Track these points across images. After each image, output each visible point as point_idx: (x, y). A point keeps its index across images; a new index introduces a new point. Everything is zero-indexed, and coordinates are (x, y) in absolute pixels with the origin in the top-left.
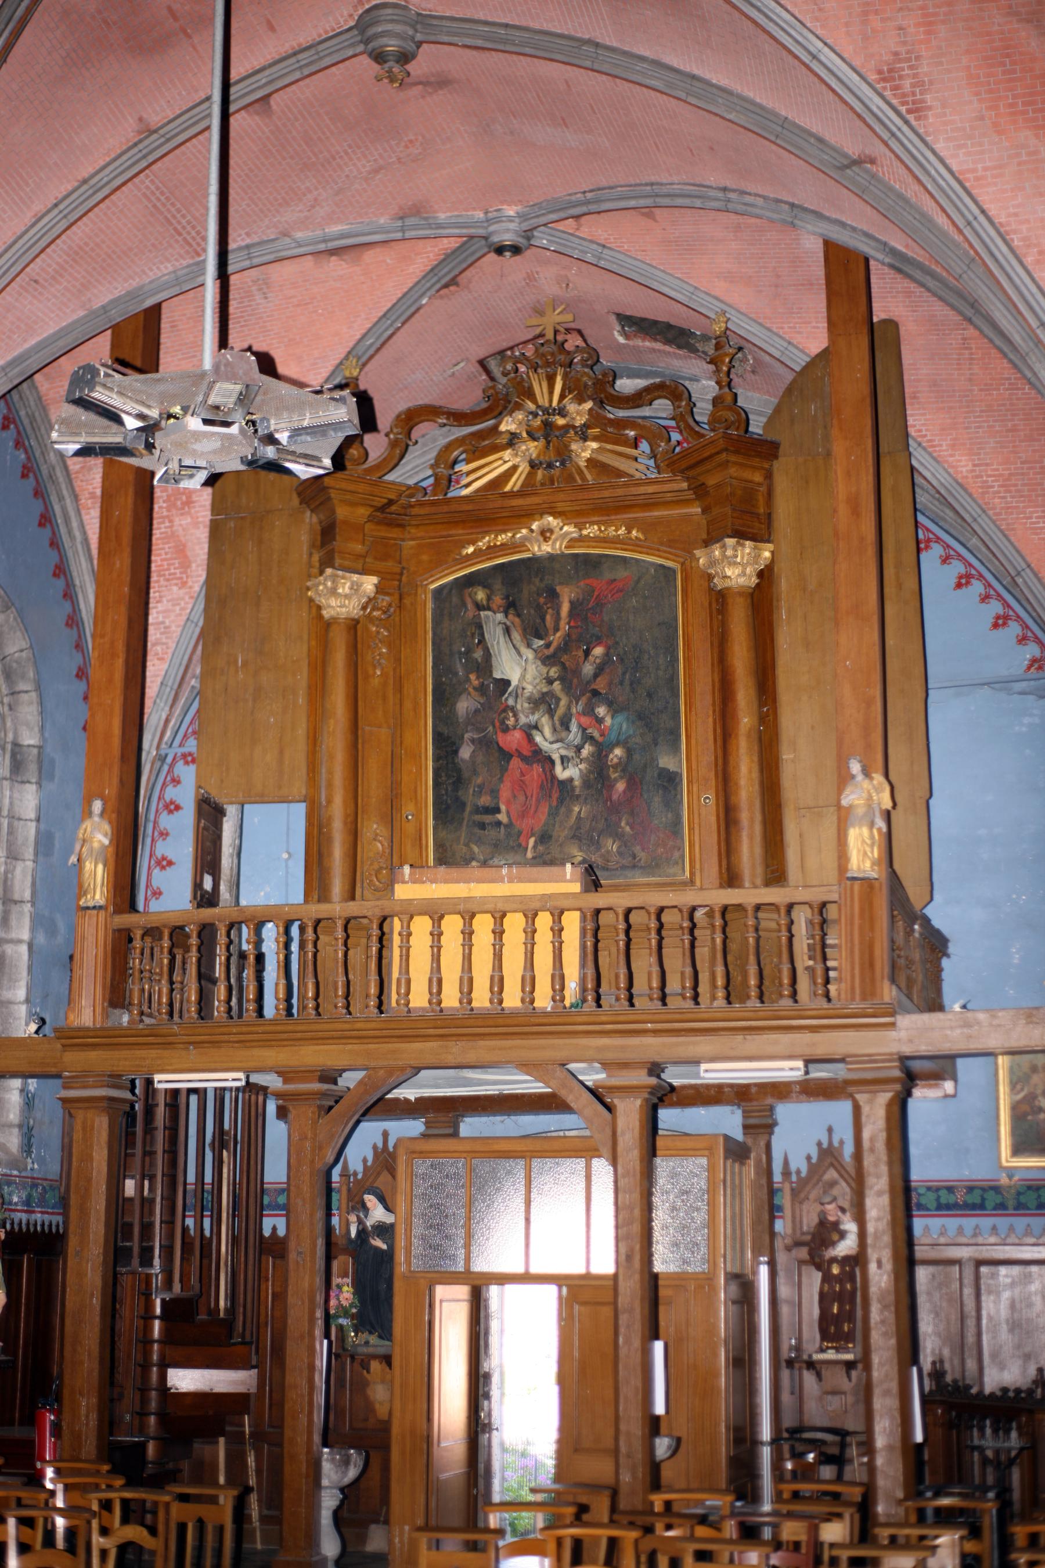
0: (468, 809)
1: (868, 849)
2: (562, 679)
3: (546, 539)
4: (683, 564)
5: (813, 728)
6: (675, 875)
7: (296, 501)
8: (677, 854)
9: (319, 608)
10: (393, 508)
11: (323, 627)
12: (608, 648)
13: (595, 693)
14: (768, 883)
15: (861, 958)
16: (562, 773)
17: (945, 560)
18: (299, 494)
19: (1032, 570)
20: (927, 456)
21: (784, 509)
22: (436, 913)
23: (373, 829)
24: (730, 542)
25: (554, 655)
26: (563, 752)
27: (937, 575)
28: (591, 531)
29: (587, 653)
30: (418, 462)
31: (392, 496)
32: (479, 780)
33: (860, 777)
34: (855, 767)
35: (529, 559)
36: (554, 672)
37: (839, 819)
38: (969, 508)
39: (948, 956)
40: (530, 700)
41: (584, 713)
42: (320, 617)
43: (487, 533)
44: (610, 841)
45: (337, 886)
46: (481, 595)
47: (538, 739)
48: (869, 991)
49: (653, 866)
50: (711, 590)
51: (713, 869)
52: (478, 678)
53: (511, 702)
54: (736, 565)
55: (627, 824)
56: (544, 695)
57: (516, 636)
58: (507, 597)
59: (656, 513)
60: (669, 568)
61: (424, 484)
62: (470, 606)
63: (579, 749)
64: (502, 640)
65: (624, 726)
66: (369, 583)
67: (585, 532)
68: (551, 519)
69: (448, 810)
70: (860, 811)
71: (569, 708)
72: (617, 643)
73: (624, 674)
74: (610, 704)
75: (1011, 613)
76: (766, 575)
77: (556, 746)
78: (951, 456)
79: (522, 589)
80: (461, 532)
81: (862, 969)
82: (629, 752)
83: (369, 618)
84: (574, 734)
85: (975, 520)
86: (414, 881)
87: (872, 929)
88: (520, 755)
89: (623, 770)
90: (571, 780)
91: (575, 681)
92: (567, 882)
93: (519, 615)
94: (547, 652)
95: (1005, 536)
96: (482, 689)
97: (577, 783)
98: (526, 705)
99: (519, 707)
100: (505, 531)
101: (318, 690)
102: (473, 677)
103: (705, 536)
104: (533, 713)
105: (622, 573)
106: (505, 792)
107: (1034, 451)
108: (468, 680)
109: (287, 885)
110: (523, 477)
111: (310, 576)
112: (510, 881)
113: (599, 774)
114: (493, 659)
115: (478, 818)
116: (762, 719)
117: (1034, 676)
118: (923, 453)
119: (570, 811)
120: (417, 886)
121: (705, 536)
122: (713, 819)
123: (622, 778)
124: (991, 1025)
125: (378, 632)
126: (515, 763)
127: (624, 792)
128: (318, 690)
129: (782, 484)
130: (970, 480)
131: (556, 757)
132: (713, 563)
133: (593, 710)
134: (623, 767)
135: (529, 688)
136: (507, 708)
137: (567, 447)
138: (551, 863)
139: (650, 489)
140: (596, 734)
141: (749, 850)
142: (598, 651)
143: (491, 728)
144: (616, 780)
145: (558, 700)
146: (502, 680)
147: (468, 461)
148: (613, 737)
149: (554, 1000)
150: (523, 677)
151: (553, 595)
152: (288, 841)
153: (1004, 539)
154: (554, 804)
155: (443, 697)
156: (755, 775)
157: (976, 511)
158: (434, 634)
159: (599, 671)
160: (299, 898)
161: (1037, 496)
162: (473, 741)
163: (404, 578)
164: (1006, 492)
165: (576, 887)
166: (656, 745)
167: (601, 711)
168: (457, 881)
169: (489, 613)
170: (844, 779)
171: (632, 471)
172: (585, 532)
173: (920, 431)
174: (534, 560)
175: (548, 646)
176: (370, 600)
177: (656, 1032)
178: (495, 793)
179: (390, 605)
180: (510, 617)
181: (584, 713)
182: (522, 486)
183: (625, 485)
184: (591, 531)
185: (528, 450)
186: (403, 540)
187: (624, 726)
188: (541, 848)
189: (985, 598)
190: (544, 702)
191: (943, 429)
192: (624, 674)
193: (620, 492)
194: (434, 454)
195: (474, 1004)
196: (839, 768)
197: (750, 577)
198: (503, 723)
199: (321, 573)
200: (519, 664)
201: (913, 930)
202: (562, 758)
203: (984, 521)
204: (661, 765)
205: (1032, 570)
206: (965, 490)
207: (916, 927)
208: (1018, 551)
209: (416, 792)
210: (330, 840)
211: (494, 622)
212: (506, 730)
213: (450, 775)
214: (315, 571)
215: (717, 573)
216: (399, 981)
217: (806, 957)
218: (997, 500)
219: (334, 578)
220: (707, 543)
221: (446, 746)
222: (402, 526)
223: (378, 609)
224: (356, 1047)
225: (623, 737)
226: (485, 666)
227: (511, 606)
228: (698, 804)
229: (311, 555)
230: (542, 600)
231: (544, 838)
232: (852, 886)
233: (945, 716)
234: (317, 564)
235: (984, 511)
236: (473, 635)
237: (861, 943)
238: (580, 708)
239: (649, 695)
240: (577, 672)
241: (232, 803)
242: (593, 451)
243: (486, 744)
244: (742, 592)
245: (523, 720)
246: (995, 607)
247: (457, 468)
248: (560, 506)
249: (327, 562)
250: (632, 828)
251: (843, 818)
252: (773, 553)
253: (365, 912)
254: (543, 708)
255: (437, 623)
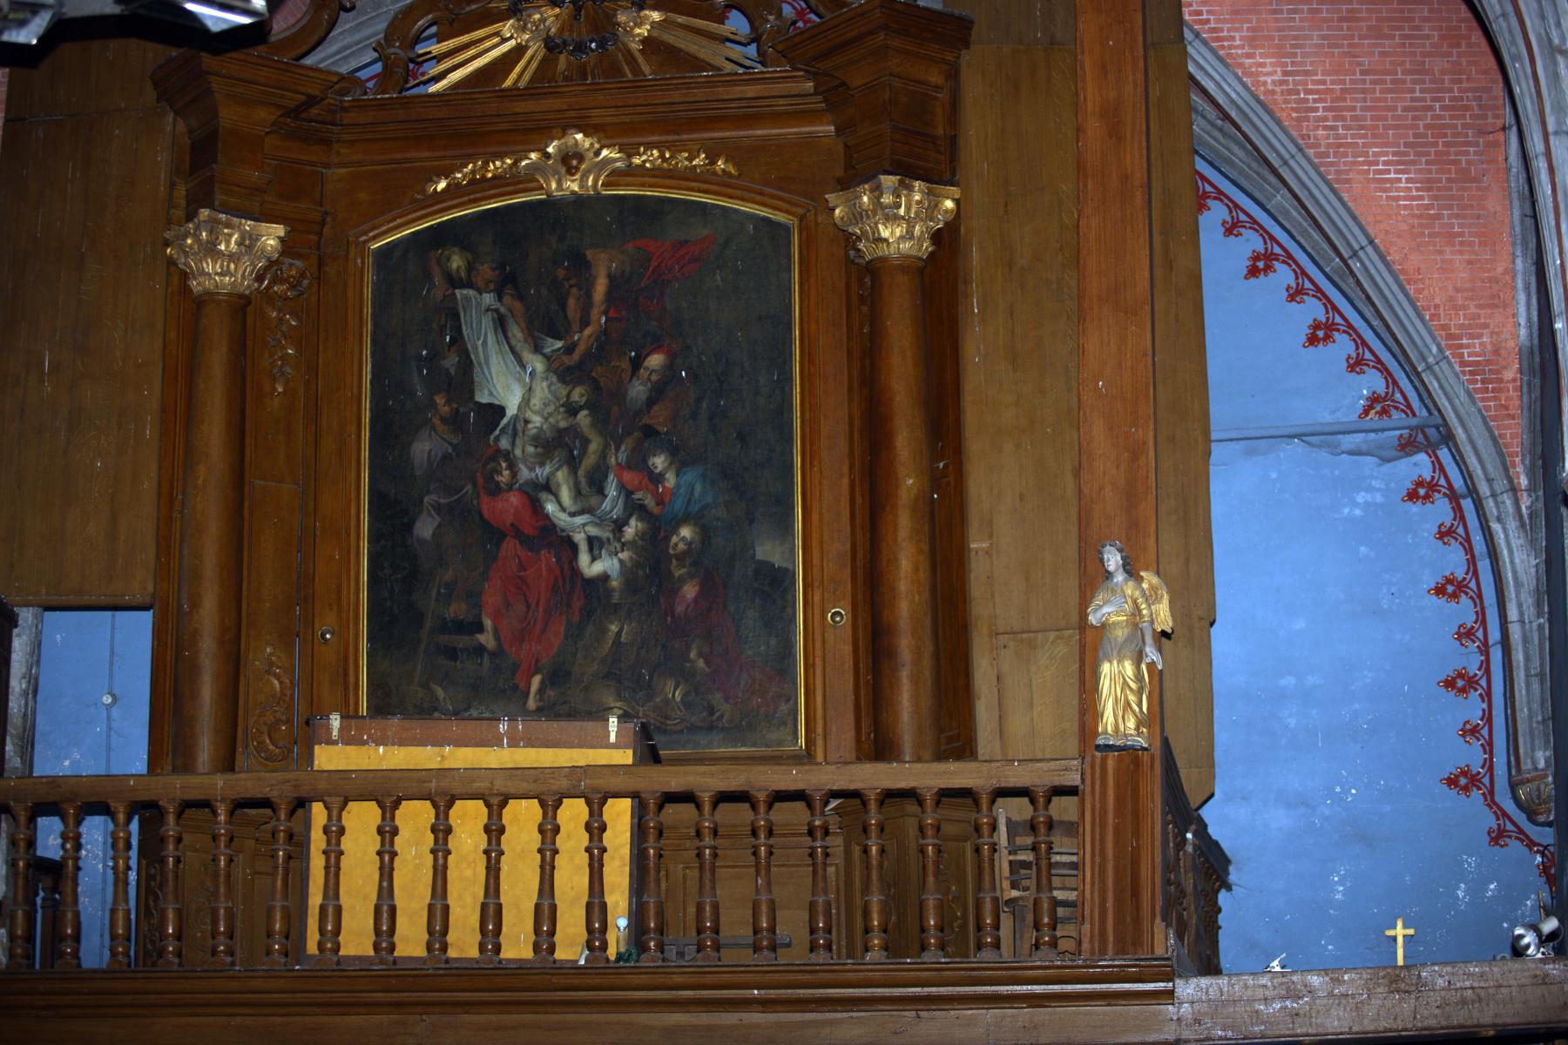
0: (428, 625)
1: (1132, 698)
2: (591, 406)
3: (571, 171)
4: (802, 218)
5: (1022, 497)
6: (780, 744)
7: (150, 95)
8: (784, 708)
9: (185, 276)
10: (314, 111)
11: (190, 307)
12: (672, 356)
13: (650, 432)
14: (940, 756)
15: (1117, 882)
16: (591, 567)
17: (1231, 229)
18: (156, 85)
19: (1376, 248)
20: (1209, 56)
21: (977, 129)
22: (388, 793)
23: (263, 652)
24: (889, 181)
25: (580, 365)
26: (593, 531)
27: (1221, 256)
28: (647, 158)
29: (637, 364)
30: (349, 40)
31: (315, 91)
32: (448, 576)
33: (1120, 577)
34: (1113, 560)
35: (540, 202)
36: (578, 394)
37: (1083, 647)
38: (1277, 146)
39: (1229, 888)
40: (537, 440)
41: (629, 466)
42: (187, 290)
43: (471, 158)
44: (670, 684)
45: (205, 750)
46: (457, 262)
47: (550, 507)
48: (1130, 937)
49: (742, 728)
50: (849, 262)
51: (844, 733)
52: (448, 402)
53: (504, 444)
54: (898, 222)
55: (700, 654)
56: (561, 433)
57: (516, 333)
58: (502, 267)
59: (759, 132)
60: (779, 224)
61: (363, 75)
62: (438, 279)
63: (619, 525)
64: (491, 339)
65: (698, 488)
66: (271, 237)
67: (637, 161)
68: (579, 136)
69: (393, 625)
70: (1120, 634)
71: (603, 456)
72: (688, 348)
73: (699, 400)
74: (673, 452)
75: (1338, 319)
76: (947, 239)
77: (579, 520)
78: (1248, 56)
79: (531, 256)
80: (426, 154)
81: (1118, 901)
82: (705, 533)
83: (267, 295)
84: (613, 499)
85: (1286, 163)
86: (347, 739)
87: (1137, 833)
88: (518, 534)
89: (695, 564)
90: (605, 577)
91: (615, 409)
92: (610, 747)
93: (521, 298)
94: (569, 361)
95: (1333, 191)
96: (456, 421)
97: (615, 584)
98: (530, 449)
99: (518, 452)
100: (501, 156)
101: (180, 416)
102: (440, 400)
103: (840, 172)
104: (542, 464)
105: (699, 232)
106: (492, 596)
107: (1382, 54)
108: (433, 405)
109: (109, 748)
110: (534, 65)
111: (169, 222)
112: (513, 744)
113: (653, 563)
114: (477, 370)
115: (444, 639)
116: (936, 480)
117: (1375, 425)
118: (1203, 49)
119: (605, 631)
120: (351, 749)
121: (840, 172)
122: (847, 649)
123: (692, 577)
124: (1331, 995)
125: (281, 320)
126: (510, 547)
127: (696, 599)
128: (180, 416)
129: (974, 86)
130: (1278, 97)
131: (579, 538)
132: (858, 215)
133: (645, 461)
134: (693, 556)
135: (537, 420)
136: (499, 454)
137: (610, 18)
138: (572, 715)
139: (751, 91)
140: (650, 502)
141: (908, 703)
142: (655, 360)
143: (469, 487)
144: (682, 580)
145: (586, 442)
146: (491, 405)
147: (441, 38)
148: (679, 505)
149: (589, 945)
150: (526, 402)
151: (581, 265)
152: (111, 676)
153: (1331, 197)
154: (576, 619)
155: (390, 433)
156: (923, 575)
157: (1284, 147)
158: (376, 325)
159: (657, 394)
160: (139, 765)
161: (1386, 128)
162: (438, 508)
163: (327, 231)
164: (1336, 119)
165: (626, 757)
166: (752, 521)
167: (659, 462)
168: (422, 743)
169: (471, 292)
170: (1093, 579)
171: (720, 62)
172: (637, 161)
173: (1199, 13)
174: (550, 204)
175: (569, 350)
176: (271, 263)
177: (766, 1004)
178: (474, 598)
179: (303, 275)
180: (507, 299)
181: (629, 466)
182: (532, 80)
183: (709, 83)
184: (647, 158)
185: (543, 20)
186: (327, 166)
187: (698, 488)
188: (551, 693)
189: (1295, 295)
190: (559, 444)
191: (1236, 12)
192: (699, 400)
193: (699, 94)
194: (383, 25)
195: (452, 953)
196: (1082, 560)
197: (920, 240)
198: (490, 478)
199: (191, 216)
200: (520, 380)
201: (1185, 839)
202: (591, 541)
203: (1300, 166)
204: (759, 556)
205: (1376, 248)
206: (1270, 113)
207: (1189, 836)
208: (1354, 218)
209: (339, 592)
210: (194, 670)
211: (478, 306)
212: (496, 491)
213: (397, 564)
214: (179, 213)
215: (864, 233)
216: (323, 908)
217: (1006, 884)
218: (1321, 132)
219: (213, 226)
220: (847, 183)
221: (392, 517)
222: (327, 143)
223: (283, 281)
224: (249, 1020)
225: (695, 508)
226: (463, 380)
227: (506, 282)
228: (820, 621)
229: (173, 185)
230: (561, 273)
231: (557, 676)
232: (1104, 760)
233: (1236, 489)
234: (183, 202)
235: (1301, 150)
236: (442, 329)
237: (1117, 857)
238: (622, 457)
239: (742, 437)
240: (618, 395)
241: (27, 605)
242: (653, 24)
243: (458, 513)
244: (908, 266)
245: (525, 474)
246: (1313, 310)
247: (421, 49)
248: (597, 116)
249: (202, 197)
250: (707, 663)
251: (1089, 648)
252: (957, 202)
253: (265, 792)
254: (559, 455)
255: (381, 306)
